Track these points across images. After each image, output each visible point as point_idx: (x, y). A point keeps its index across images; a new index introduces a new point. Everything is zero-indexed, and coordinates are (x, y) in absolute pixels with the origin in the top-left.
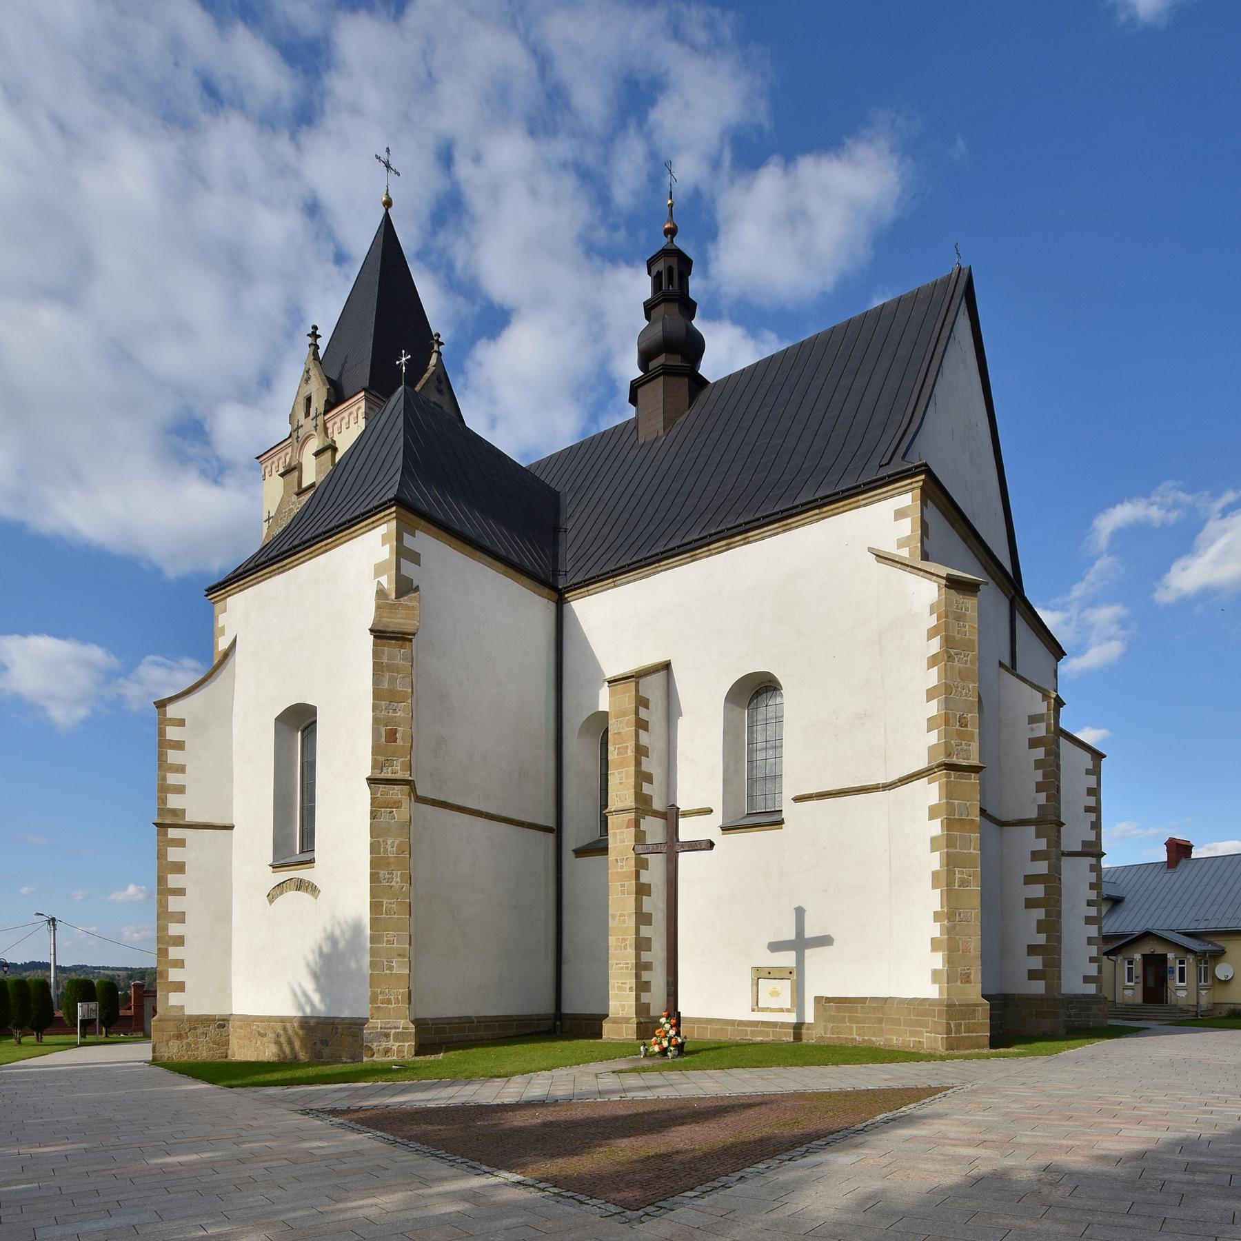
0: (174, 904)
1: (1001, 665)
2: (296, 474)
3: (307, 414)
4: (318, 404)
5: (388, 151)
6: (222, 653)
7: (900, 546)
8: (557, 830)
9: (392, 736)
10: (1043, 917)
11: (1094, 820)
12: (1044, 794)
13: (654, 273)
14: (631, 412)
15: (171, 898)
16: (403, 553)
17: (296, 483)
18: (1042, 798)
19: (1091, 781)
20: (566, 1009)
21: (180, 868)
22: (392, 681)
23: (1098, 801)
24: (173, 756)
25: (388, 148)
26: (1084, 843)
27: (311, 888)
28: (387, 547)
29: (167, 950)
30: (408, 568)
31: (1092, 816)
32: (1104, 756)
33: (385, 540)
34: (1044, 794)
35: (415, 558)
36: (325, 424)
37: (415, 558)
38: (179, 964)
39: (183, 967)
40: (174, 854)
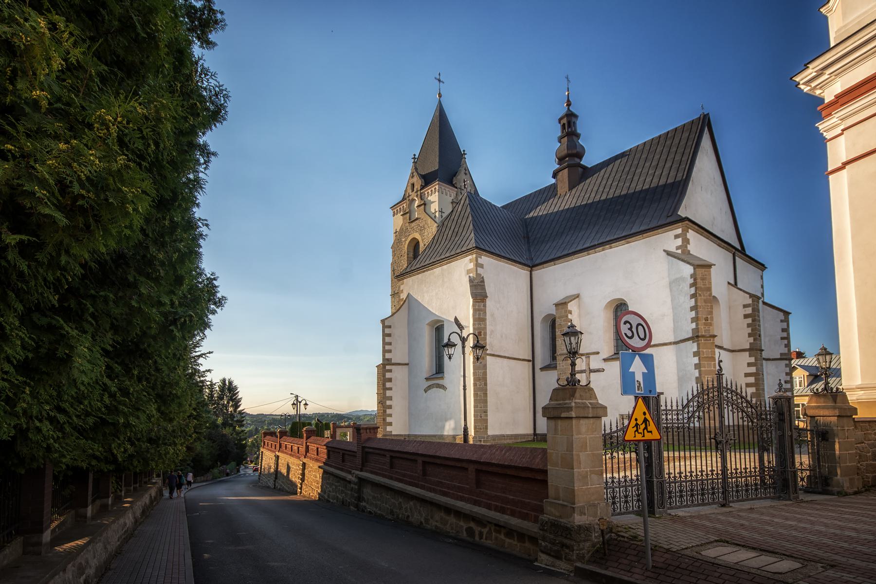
0: (388, 393)
1: (729, 283)
3: (413, 191)
4: (417, 187)
5: (439, 74)
6: (436, 318)
7: (677, 249)
8: (533, 361)
10: (755, 391)
11: (786, 343)
12: (752, 338)
13: (562, 124)
14: (553, 181)
15: (387, 391)
16: (478, 265)
17: (408, 218)
18: (751, 340)
19: (784, 325)
20: (538, 432)
21: (390, 380)
22: (480, 314)
23: (788, 334)
26: (781, 354)
27: (443, 387)
30: (480, 270)
31: (786, 342)
33: (471, 261)
34: (752, 338)
35: (482, 266)
36: (421, 193)
38: (390, 415)
39: (391, 417)
40: (388, 375)
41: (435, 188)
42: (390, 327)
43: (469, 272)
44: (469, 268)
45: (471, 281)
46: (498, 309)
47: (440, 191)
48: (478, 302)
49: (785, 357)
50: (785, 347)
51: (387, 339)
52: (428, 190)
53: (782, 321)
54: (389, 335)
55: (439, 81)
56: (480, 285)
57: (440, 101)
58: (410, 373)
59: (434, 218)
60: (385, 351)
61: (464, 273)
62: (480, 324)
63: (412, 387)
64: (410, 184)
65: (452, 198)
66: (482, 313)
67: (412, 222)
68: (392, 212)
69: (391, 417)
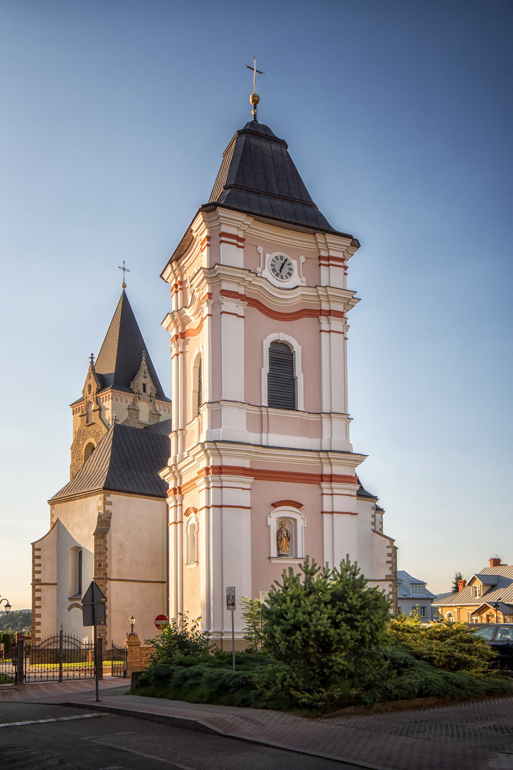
2: (85, 417)
3: (90, 393)
4: (94, 389)
9: (100, 565)
16: (106, 503)
17: (85, 421)
19: (390, 551)
22: (100, 549)
24: (37, 628)
25: (124, 262)
26: (387, 576)
28: (101, 502)
29: (35, 627)
30: (108, 508)
32: (394, 541)
36: (97, 397)
37: (110, 503)
38: (39, 631)
39: (40, 632)
41: (109, 395)
42: (39, 550)
43: (99, 508)
44: (99, 505)
45: (100, 517)
46: (128, 540)
47: (114, 399)
48: (99, 538)
49: (389, 578)
50: (390, 570)
51: (37, 561)
52: (103, 395)
53: (388, 547)
54: (39, 557)
55: (124, 269)
56: (107, 521)
57: (124, 292)
58: (58, 591)
59: (108, 426)
60: (34, 572)
61: (96, 509)
62: (100, 557)
63: (59, 606)
64: (87, 385)
65: (129, 403)
66: (102, 547)
67: (89, 426)
68: (71, 410)
69: (40, 632)
